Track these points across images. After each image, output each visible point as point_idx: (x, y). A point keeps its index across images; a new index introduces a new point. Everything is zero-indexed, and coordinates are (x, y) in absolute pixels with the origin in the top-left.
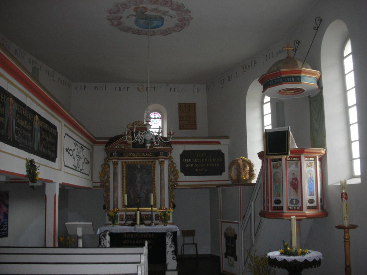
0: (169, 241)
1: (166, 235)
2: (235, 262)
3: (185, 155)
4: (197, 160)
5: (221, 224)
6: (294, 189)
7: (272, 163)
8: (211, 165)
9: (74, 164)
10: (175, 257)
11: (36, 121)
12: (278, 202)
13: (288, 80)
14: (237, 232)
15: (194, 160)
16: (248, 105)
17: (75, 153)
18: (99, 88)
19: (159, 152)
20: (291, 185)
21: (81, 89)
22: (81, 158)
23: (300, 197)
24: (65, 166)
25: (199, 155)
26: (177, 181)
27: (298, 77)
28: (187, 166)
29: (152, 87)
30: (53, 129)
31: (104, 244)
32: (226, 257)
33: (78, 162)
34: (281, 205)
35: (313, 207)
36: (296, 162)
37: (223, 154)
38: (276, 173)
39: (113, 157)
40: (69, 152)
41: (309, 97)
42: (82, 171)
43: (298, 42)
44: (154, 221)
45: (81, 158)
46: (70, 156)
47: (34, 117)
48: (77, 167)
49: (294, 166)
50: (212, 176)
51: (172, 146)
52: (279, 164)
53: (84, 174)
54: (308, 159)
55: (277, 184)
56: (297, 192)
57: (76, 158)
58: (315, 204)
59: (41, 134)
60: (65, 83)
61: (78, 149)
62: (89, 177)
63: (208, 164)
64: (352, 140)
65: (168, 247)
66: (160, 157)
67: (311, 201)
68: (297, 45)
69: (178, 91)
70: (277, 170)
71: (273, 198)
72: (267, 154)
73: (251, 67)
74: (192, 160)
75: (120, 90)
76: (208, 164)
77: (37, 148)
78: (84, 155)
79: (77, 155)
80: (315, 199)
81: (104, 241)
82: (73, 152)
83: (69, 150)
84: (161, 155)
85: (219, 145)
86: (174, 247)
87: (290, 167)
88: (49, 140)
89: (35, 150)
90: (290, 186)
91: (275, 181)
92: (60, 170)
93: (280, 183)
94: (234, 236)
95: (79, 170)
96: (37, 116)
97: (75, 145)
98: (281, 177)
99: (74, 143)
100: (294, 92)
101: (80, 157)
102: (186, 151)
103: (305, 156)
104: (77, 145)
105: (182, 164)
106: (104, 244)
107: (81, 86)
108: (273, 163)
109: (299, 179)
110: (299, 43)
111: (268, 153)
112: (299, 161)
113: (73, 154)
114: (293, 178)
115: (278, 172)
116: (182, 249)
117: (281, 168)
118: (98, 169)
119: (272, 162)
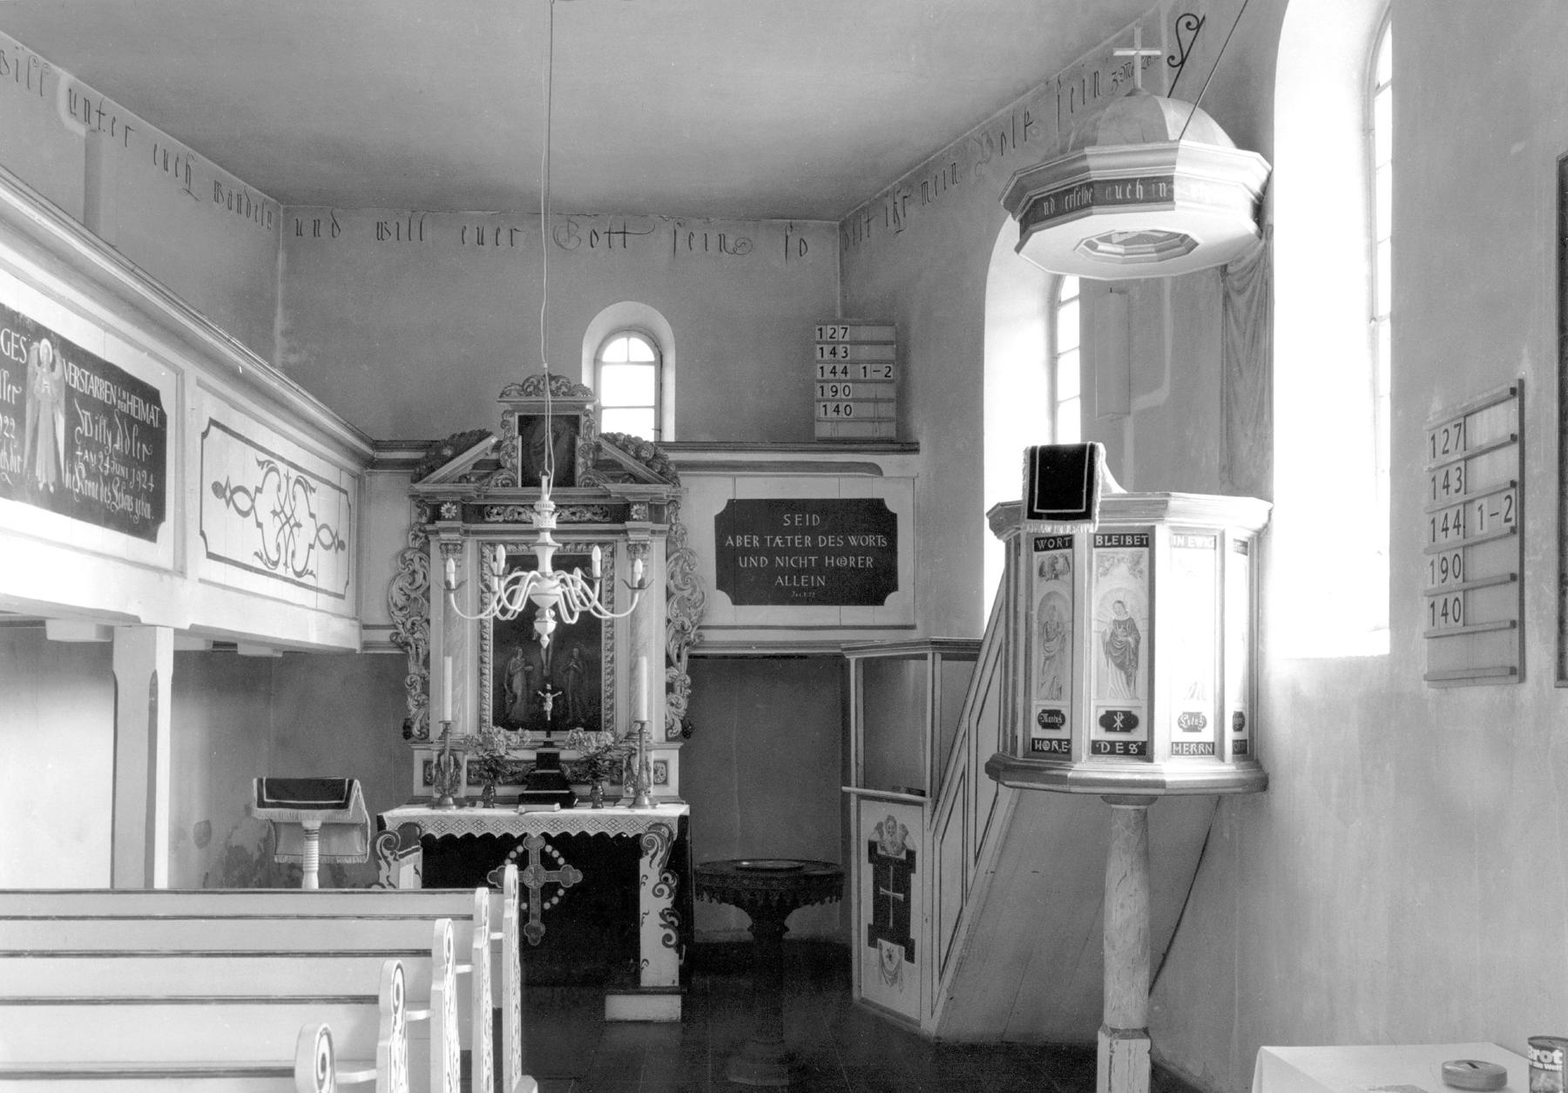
0: (650, 869)
1: (675, 842)
2: (906, 964)
3: (735, 518)
4: (785, 542)
5: (858, 806)
6: (1121, 666)
7: (1036, 554)
8: (842, 562)
9: (259, 548)
10: (673, 935)
11: (40, 363)
12: (1052, 719)
13: (1119, 196)
14: (914, 842)
15: (772, 541)
16: (995, 310)
17: (265, 503)
18: (394, 233)
19: (628, 506)
20: (1107, 653)
21: (316, 232)
22: (298, 525)
23: (1144, 704)
24: (211, 556)
25: (793, 520)
26: (704, 623)
27: (1160, 179)
28: (743, 563)
29: (622, 235)
30: (141, 401)
31: (388, 877)
32: (872, 942)
33: (281, 540)
34: (1062, 733)
35: (1201, 747)
36: (1133, 553)
37: (893, 518)
38: (1049, 595)
39: (439, 524)
40: (230, 501)
41: (1224, 269)
42: (305, 579)
43: (1194, 25)
44: (464, 791)
45: (298, 525)
46: (240, 518)
47: (28, 345)
48: (275, 564)
49: (1123, 568)
50: (843, 607)
51: (681, 479)
52: (1061, 561)
53: (317, 590)
54: (1186, 541)
55: (1054, 645)
56: (1130, 679)
57: (272, 525)
58: (1207, 735)
59: (73, 421)
60: (249, 206)
61: (279, 490)
62: (346, 606)
63: (829, 559)
64: (652, 411)
65: (645, 893)
66: (628, 524)
67: (1193, 723)
68: (1187, 36)
69: (722, 246)
70: (1052, 586)
71: (1034, 703)
72: (1032, 515)
73: (1010, 143)
74: (762, 541)
75: (481, 242)
76: (829, 559)
77: (52, 478)
78: (313, 511)
79: (275, 513)
80: (1210, 714)
81: (389, 864)
82: (253, 501)
83: (233, 492)
84: (635, 517)
85: (878, 481)
86: (670, 896)
87: (1105, 574)
88: (117, 446)
89: (41, 486)
90: (1103, 655)
91: (1047, 634)
92: (181, 572)
93: (1064, 639)
94: (903, 856)
95: (291, 575)
96: (45, 342)
97: (265, 470)
98: (1067, 617)
99: (261, 464)
100: (1158, 251)
101: (292, 522)
102: (740, 501)
103: (1173, 528)
104: (274, 469)
105: (727, 560)
106: (388, 877)
107: (316, 224)
108: (1038, 557)
109: (1142, 627)
110: (1198, 27)
111: (1036, 510)
112: (1146, 550)
113: (293, 515)
114: (1117, 623)
115: (1056, 593)
116: (962, 895)
117: (1068, 577)
118: (383, 567)
119: (1037, 549)
